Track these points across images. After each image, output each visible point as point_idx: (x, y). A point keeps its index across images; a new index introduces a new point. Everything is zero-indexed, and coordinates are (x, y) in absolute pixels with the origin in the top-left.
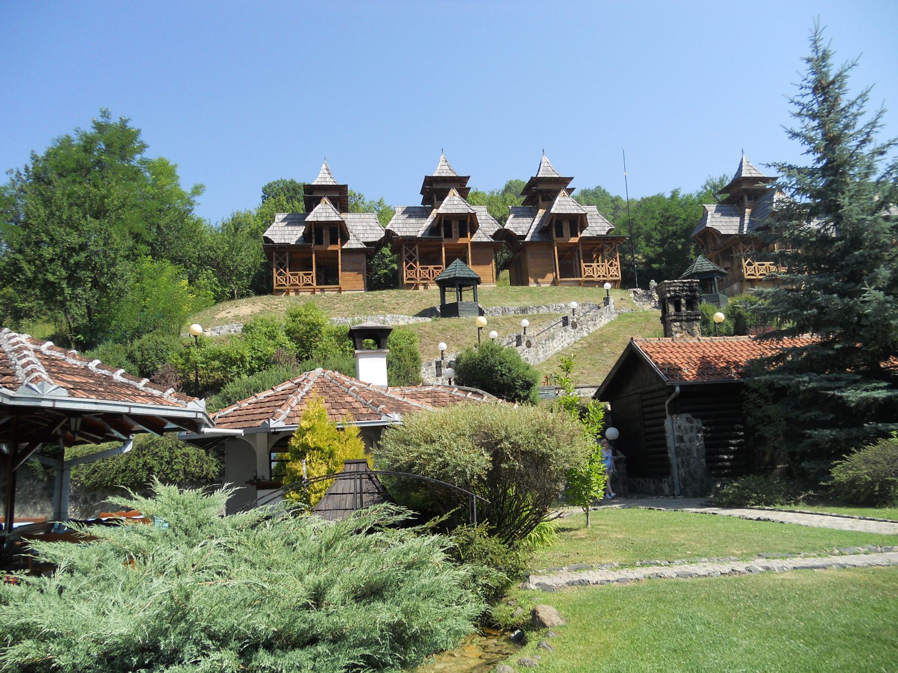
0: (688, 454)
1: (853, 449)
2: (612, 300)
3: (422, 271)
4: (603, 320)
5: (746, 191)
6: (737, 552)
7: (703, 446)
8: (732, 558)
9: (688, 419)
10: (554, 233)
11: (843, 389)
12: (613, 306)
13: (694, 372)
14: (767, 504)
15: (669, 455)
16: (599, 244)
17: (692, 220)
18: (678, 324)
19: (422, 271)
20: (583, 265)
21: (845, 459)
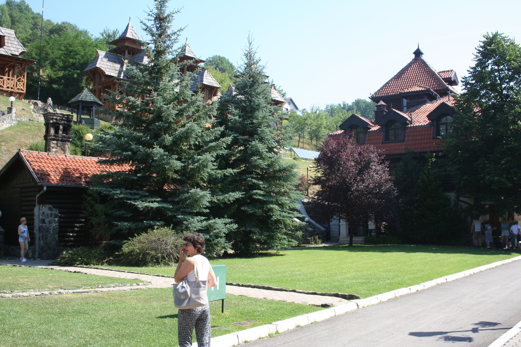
0: (47, 231)
1: (136, 235)
2: (14, 110)
4: (5, 124)
5: (127, 47)
6: (51, 287)
7: (57, 227)
8: (46, 289)
9: (50, 209)
11: (136, 200)
12: (14, 115)
13: (58, 178)
14: (86, 264)
15: (35, 231)
16: (12, 62)
17: (88, 58)
18: (55, 142)
21: (130, 240)
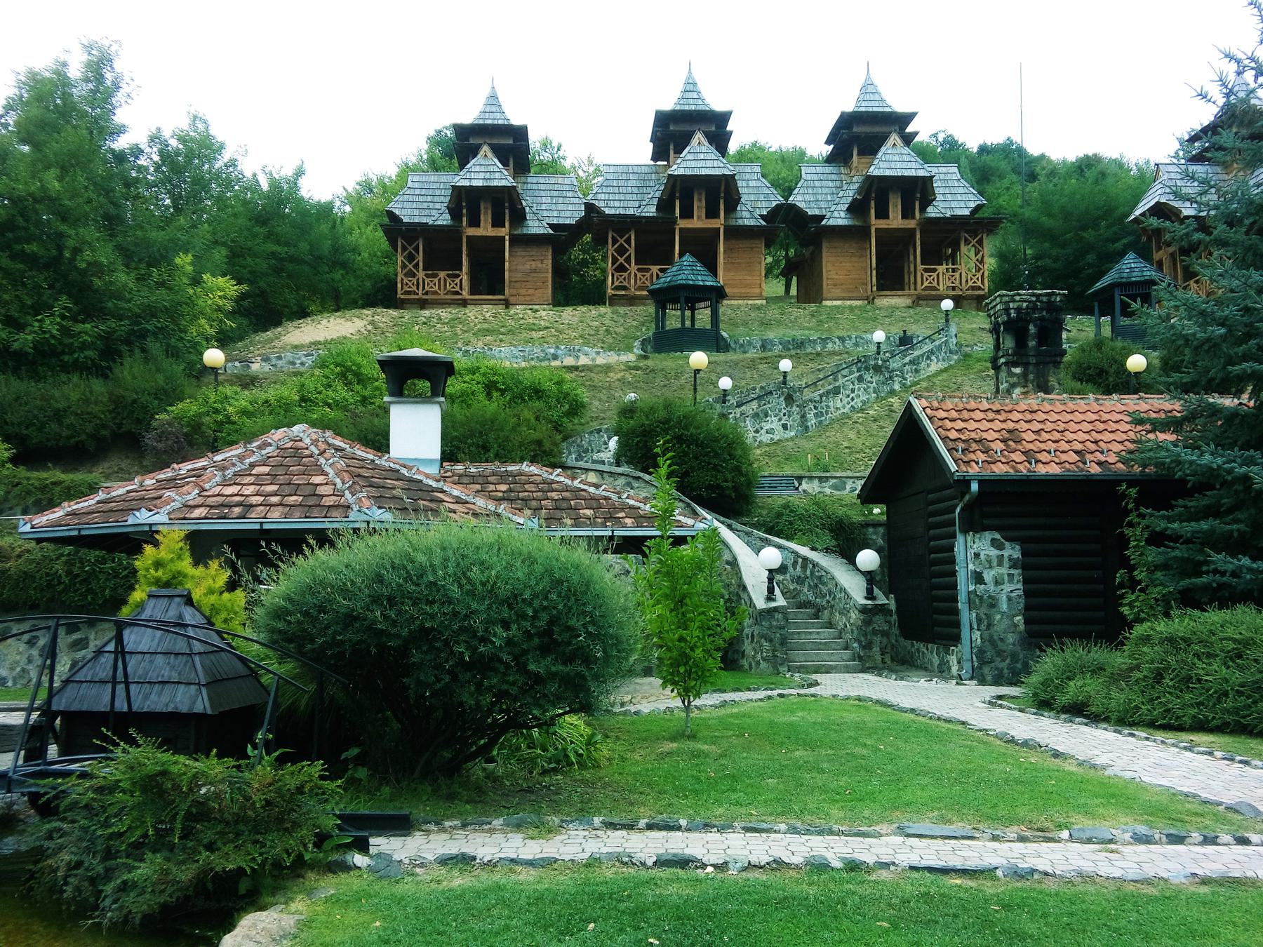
0: (992, 606)
3: (639, 275)
7: (1021, 592)
9: (994, 543)
10: (873, 212)
19: (639, 275)
20: (920, 267)
